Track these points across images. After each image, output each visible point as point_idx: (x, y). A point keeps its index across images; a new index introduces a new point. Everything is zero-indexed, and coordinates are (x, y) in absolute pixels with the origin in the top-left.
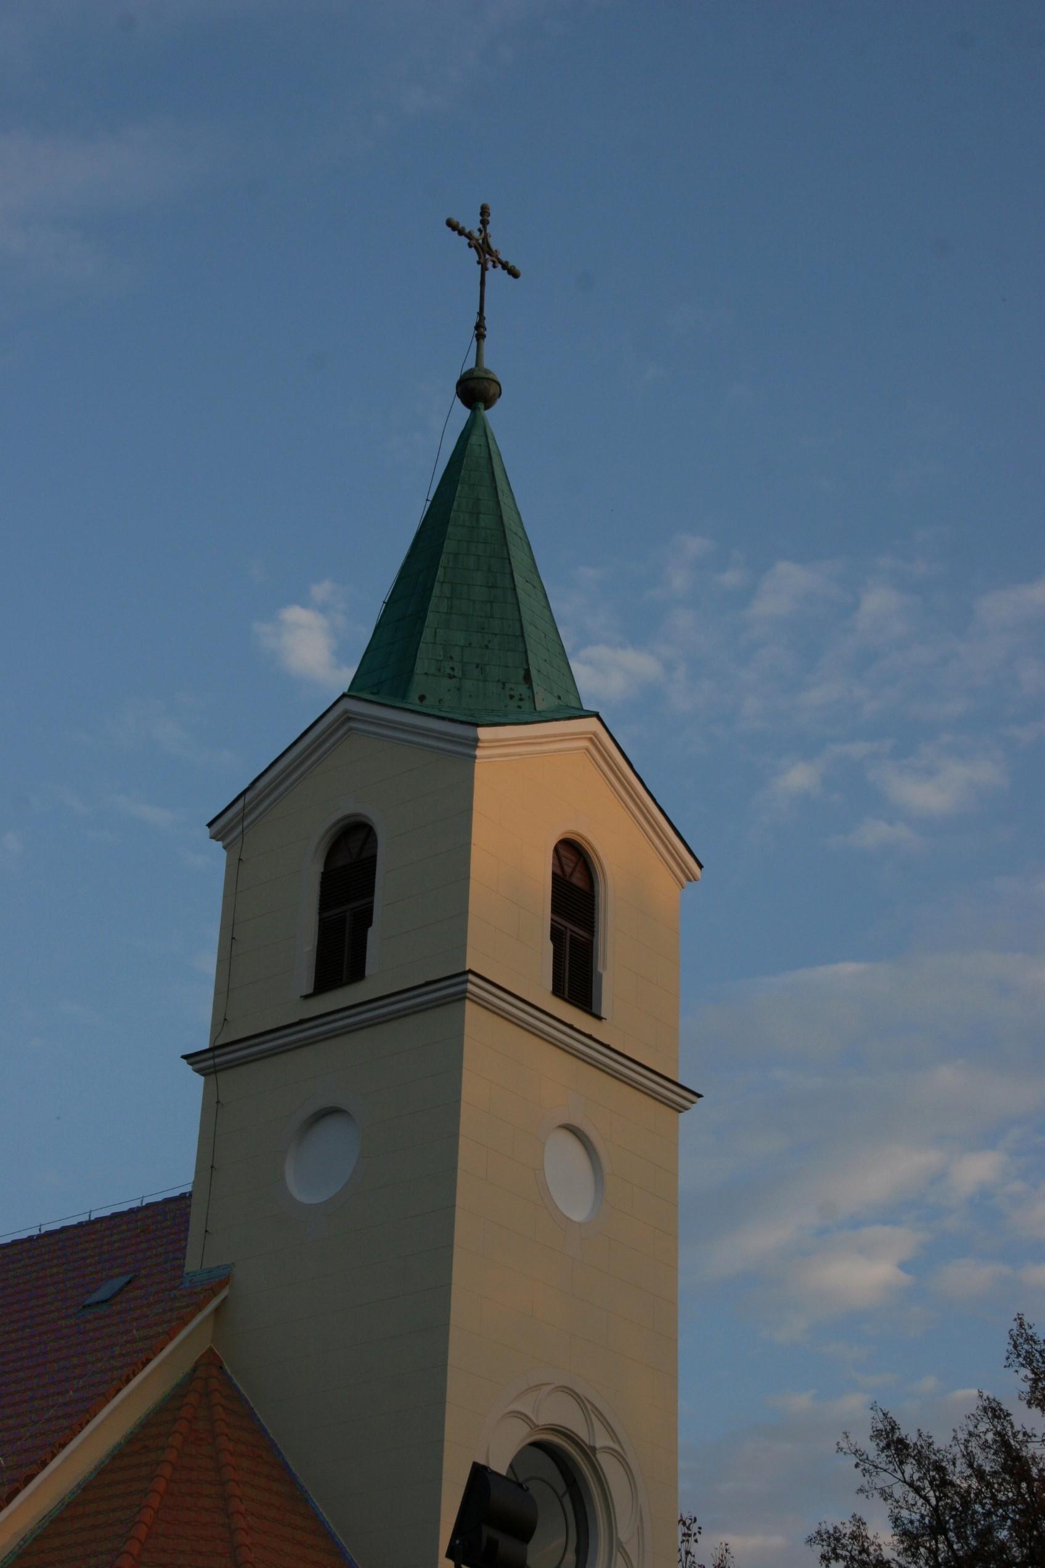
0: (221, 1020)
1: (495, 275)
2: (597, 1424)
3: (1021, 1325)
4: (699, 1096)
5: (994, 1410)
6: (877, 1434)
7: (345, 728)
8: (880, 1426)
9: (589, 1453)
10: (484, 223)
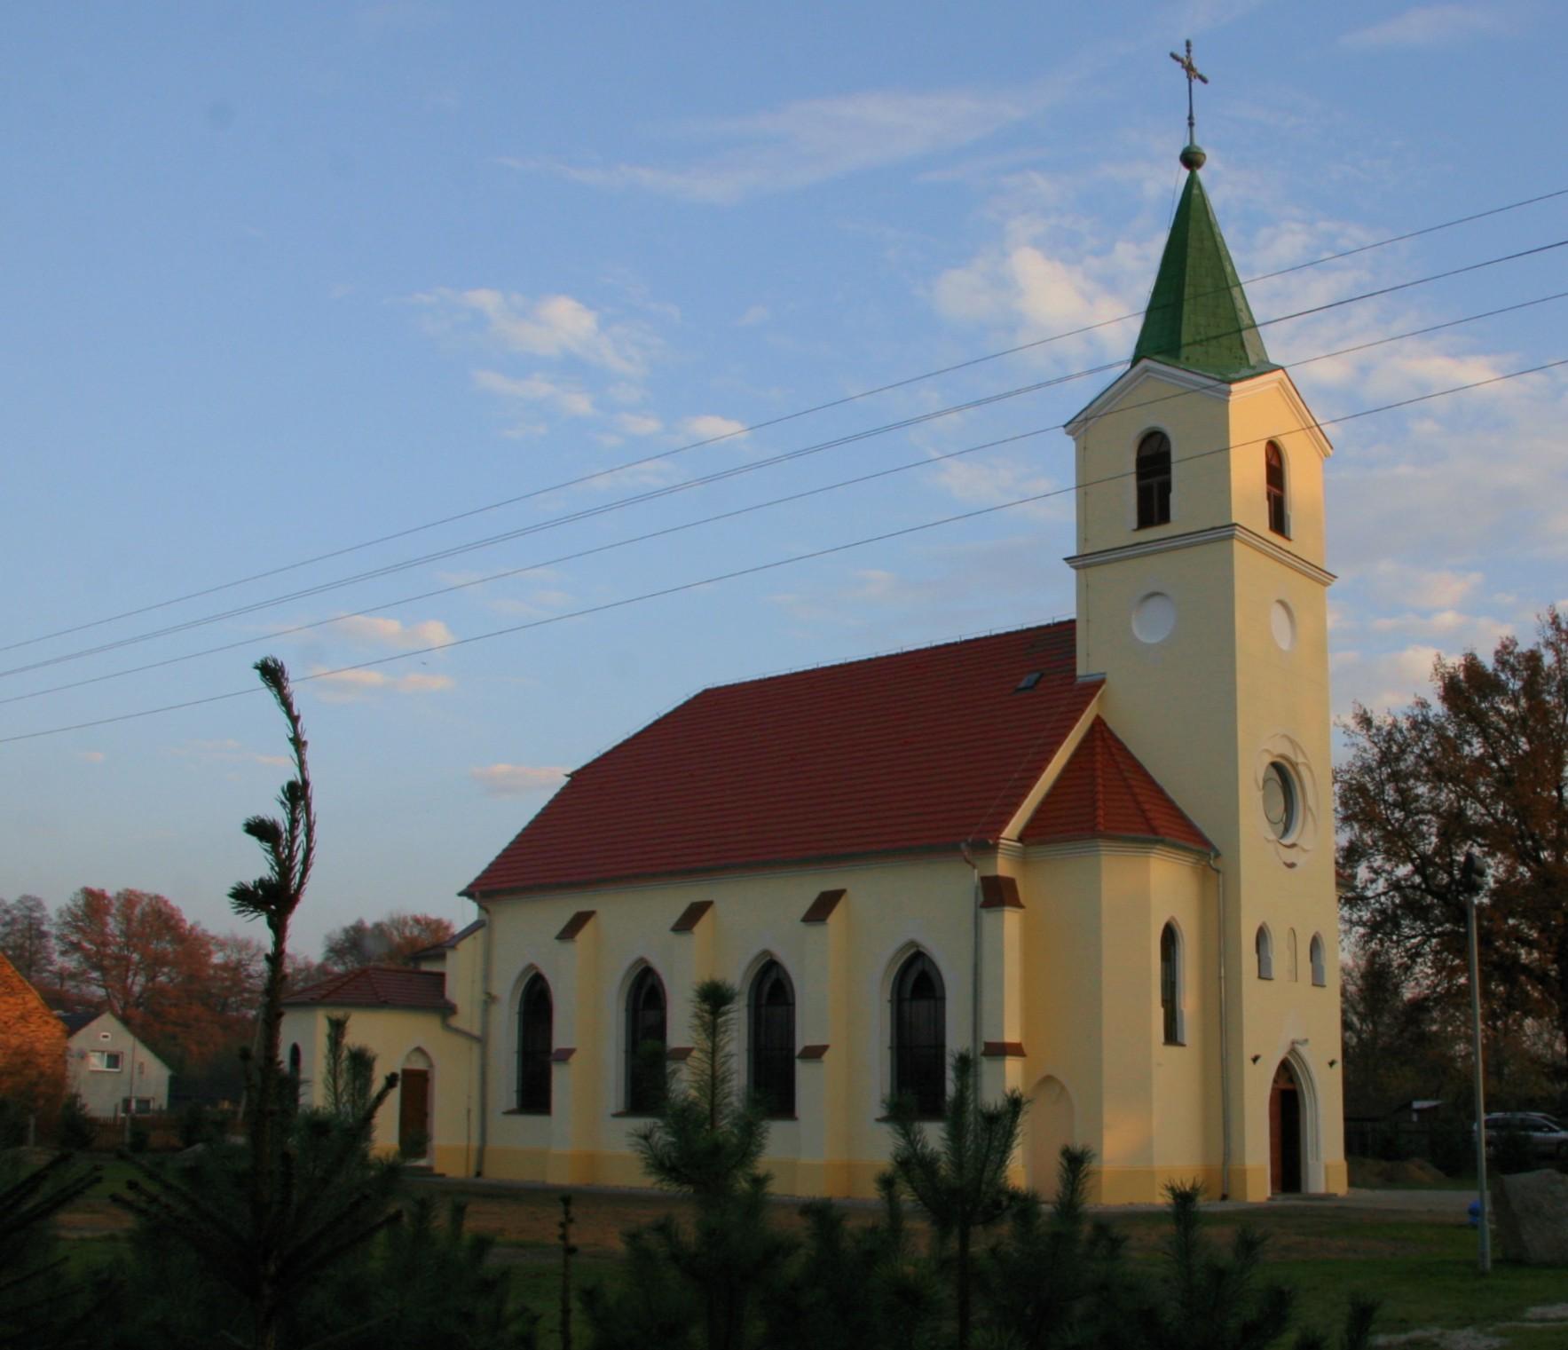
0: (1083, 538)
1: (1197, 83)
2: (1299, 752)
3: (1439, 658)
4: (1335, 577)
5: (1422, 703)
6: (1356, 716)
7: (1145, 376)
8: (1357, 712)
9: (1294, 765)
10: (1189, 51)
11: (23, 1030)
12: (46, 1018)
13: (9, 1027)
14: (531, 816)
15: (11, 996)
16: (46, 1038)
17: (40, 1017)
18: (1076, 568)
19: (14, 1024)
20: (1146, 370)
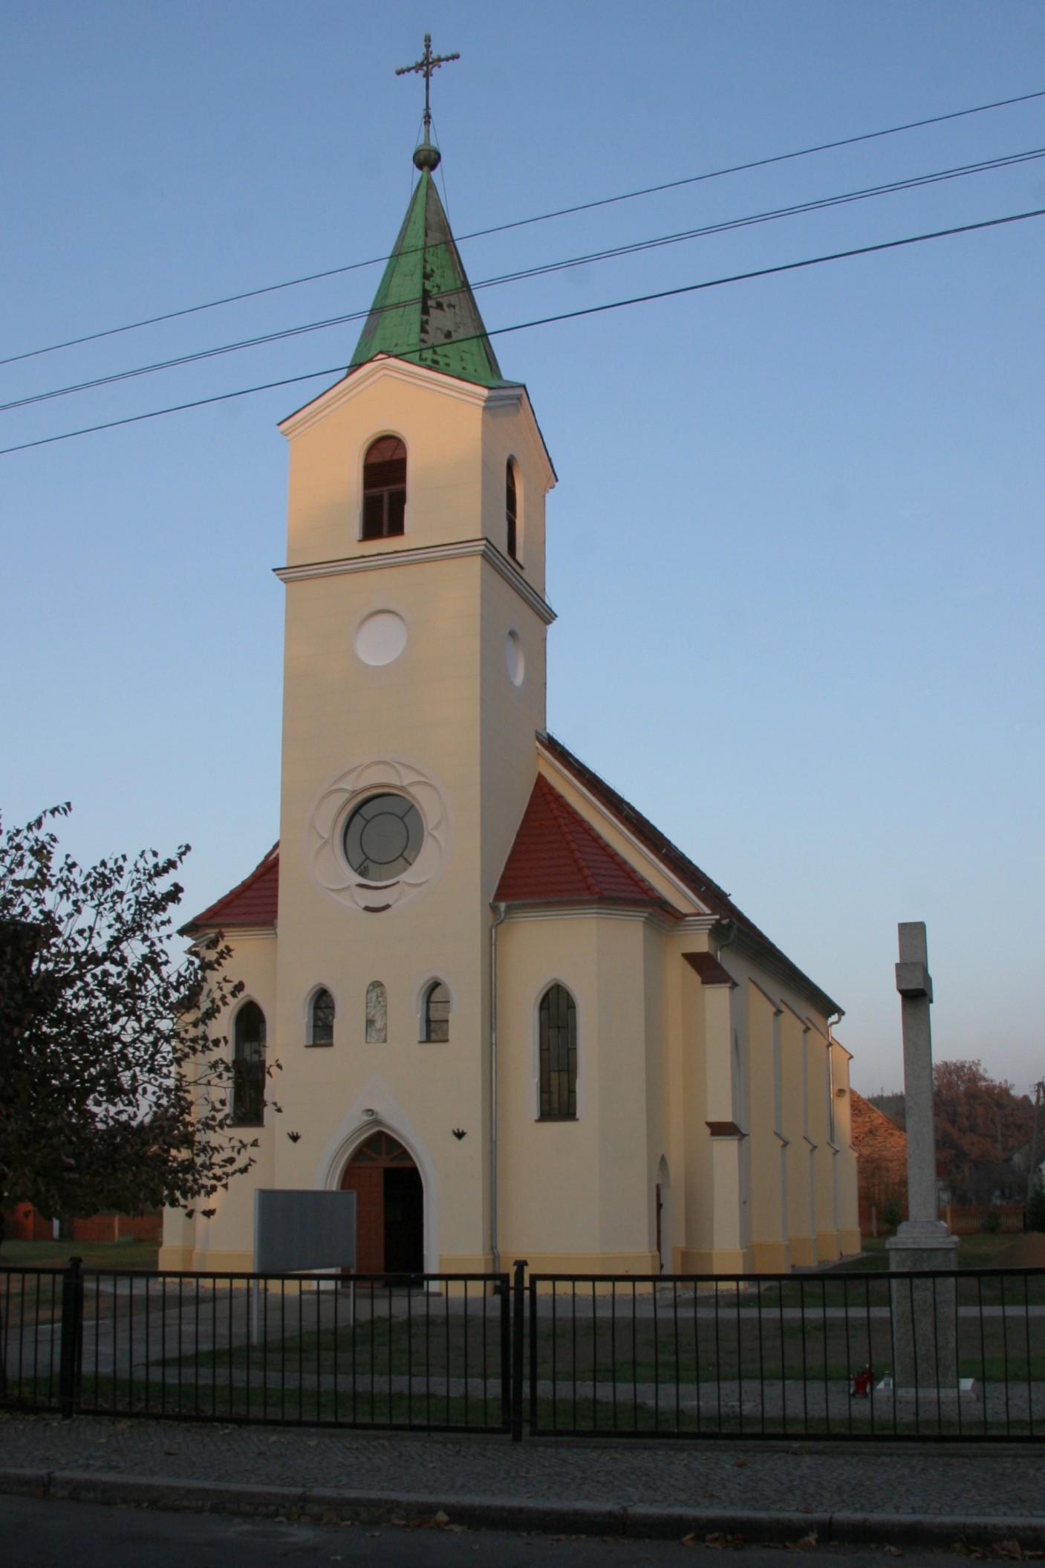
11: (871, 1143)
12: (890, 1131)
13: (860, 1141)
14: (766, 933)
15: (859, 1116)
16: (893, 1146)
17: (886, 1131)
18: (286, 581)
19: (863, 1138)
20: (385, 375)
